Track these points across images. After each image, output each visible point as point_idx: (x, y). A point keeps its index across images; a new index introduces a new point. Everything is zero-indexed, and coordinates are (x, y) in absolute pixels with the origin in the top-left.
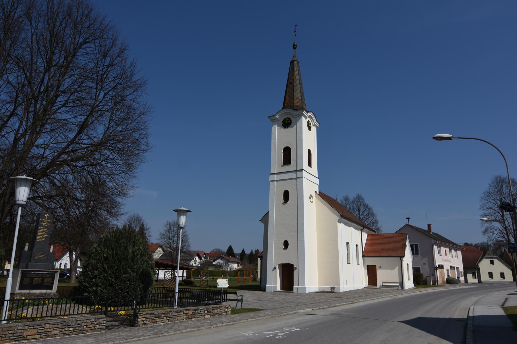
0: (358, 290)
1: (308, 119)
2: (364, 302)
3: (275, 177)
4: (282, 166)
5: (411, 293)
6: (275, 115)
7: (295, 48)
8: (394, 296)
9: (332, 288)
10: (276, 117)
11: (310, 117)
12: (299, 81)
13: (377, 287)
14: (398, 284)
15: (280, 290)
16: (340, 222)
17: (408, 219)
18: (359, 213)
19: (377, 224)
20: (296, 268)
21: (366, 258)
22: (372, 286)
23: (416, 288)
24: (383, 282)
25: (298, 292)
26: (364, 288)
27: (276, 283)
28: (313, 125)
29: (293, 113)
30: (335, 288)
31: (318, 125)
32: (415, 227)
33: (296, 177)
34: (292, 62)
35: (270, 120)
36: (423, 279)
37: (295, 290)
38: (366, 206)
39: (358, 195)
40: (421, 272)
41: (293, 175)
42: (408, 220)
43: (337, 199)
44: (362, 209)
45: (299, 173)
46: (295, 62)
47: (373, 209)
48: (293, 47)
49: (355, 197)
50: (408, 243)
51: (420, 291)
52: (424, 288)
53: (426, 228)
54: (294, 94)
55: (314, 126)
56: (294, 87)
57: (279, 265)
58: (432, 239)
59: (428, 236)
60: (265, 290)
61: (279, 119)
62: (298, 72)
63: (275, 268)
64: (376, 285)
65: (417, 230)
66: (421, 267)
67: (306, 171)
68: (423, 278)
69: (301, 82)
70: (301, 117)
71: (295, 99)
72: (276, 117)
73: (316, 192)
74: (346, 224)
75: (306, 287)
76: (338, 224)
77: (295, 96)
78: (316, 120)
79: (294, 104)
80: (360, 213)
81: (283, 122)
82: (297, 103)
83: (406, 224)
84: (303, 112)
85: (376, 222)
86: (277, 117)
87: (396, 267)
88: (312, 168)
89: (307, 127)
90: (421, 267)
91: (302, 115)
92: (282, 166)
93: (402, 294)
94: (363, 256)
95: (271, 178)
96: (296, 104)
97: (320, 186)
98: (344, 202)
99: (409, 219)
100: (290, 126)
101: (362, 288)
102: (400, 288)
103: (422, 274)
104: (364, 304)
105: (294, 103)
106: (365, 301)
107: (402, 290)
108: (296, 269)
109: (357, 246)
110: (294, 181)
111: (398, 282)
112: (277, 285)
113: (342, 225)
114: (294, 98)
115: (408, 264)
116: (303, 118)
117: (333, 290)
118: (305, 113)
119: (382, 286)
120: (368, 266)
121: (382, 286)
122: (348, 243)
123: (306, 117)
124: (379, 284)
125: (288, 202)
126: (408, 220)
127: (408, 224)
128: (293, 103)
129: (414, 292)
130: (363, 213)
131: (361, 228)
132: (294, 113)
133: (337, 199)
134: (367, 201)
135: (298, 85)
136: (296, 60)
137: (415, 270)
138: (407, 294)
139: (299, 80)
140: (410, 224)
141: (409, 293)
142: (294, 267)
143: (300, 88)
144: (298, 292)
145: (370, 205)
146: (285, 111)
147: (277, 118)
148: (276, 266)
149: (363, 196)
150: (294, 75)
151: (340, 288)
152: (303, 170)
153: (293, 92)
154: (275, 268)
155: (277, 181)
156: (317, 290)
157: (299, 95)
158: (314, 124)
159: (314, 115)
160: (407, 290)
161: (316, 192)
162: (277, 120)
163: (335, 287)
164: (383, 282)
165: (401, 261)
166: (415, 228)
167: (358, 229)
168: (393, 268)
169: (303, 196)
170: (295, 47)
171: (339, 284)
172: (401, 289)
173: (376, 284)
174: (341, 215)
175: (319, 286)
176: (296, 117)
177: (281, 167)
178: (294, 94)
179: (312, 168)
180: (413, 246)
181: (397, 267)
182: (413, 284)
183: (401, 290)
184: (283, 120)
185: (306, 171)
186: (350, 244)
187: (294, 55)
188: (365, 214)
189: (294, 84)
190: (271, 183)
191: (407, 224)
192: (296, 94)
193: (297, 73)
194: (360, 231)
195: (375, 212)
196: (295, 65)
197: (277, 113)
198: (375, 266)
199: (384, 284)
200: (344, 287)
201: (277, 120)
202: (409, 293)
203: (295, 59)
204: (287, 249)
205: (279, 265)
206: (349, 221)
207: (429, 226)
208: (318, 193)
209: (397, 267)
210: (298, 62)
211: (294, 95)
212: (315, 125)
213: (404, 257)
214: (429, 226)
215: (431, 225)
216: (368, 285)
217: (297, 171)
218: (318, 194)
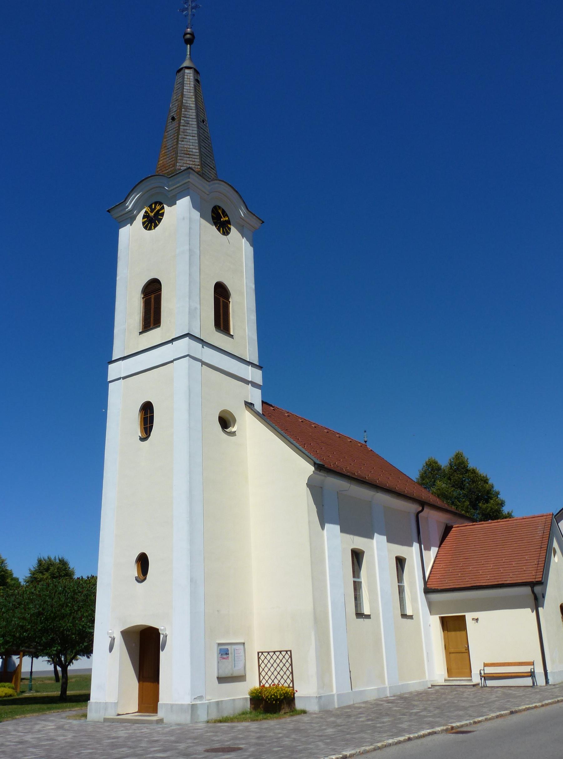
24: (486, 665)
94: (427, 591)
100: (159, 222)
144: (547, 682)
179: (232, 336)
205: (126, 634)
208: (258, 407)
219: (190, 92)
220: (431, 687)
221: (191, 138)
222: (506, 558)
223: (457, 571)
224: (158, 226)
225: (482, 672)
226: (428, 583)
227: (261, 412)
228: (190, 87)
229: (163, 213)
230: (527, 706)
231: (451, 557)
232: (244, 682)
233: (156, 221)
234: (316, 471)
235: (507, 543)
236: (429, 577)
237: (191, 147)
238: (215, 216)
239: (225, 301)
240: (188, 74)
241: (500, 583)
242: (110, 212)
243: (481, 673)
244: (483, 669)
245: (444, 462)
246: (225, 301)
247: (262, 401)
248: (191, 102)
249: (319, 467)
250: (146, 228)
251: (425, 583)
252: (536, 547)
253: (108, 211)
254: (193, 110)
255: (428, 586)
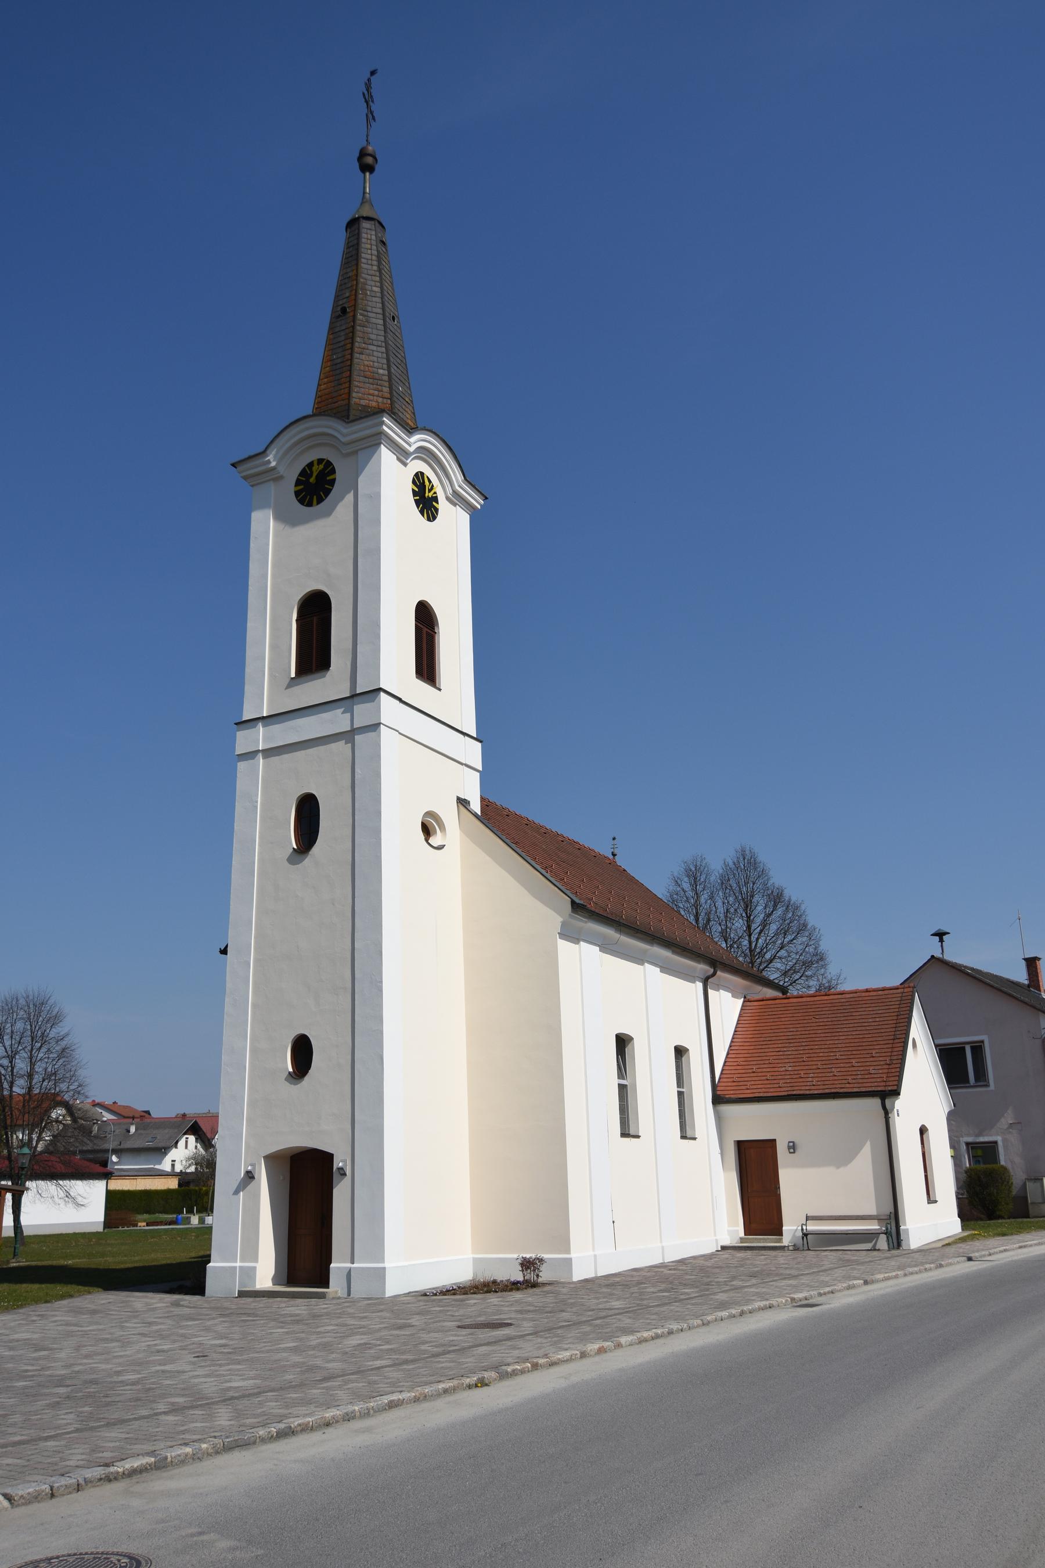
0: (682, 1262)
1: (417, 466)
2: (586, 1362)
3: (261, 737)
4: (292, 682)
5: (920, 1272)
6: (264, 453)
7: (366, 168)
8: (820, 1295)
9: (527, 1264)
10: (269, 462)
11: (424, 453)
12: (383, 303)
13: (780, 1241)
14: (874, 1226)
15: (276, 1280)
16: (570, 935)
17: (940, 935)
18: (749, 927)
19: (824, 966)
20: (342, 1173)
21: (727, 1109)
22: (759, 1241)
23: (972, 1238)
24: (808, 1218)
25: (349, 1294)
26: (724, 1248)
27: (252, 1252)
28: (448, 498)
29: (336, 434)
30: (541, 1260)
31: (477, 502)
32: (972, 969)
33: (349, 729)
34: (353, 224)
35: (245, 478)
36: (1010, 1191)
37: (336, 1285)
38: (776, 898)
39: (743, 851)
40: (1003, 1163)
41: (337, 721)
42: (941, 941)
43: (614, 855)
44: (760, 908)
45: (362, 713)
46: (365, 225)
47: (803, 907)
48: (357, 165)
49: (731, 864)
50: (918, 1029)
51: (970, 1259)
52: (1004, 1235)
53: (1021, 976)
54: (356, 355)
55: (455, 505)
56: (353, 327)
57: (272, 1160)
58: (1040, 1013)
59: (1026, 1003)
60: (199, 1289)
61: (281, 470)
62: (379, 267)
63: (250, 1176)
64: (778, 1231)
65: (975, 978)
66: (1004, 1140)
67: (400, 700)
68: (1009, 1185)
69: (389, 306)
70: (378, 449)
71: (357, 380)
72: (269, 462)
73: (463, 802)
74: (606, 947)
75: (387, 1265)
76: (563, 946)
77: (356, 367)
78: (460, 477)
79: (354, 401)
80: (754, 926)
81: (298, 483)
82: (363, 394)
83: (930, 957)
84: (383, 423)
85: (820, 958)
86: (271, 459)
87: (865, 1144)
88: (440, 690)
89: (410, 500)
90: (999, 1139)
91: (376, 439)
92: (292, 682)
93: (866, 1283)
94: (718, 1100)
95: (244, 740)
96: (363, 402)
97: (486, 777)
98: (686, 886)
99: (945, 938)
100: (327, 495)
101: (710, 1248)
102: (882, 1242)
103: (1005, 1169)
104: (562, 1383)
105: (354, 395)
106: (601, 1351)
107: (895, 1252)
108: (345, 1174)
109: (680, 1052)
110: (341, 748)
111: (873, 1211)
112: (256, 1259)
113: (589, 951)
114: (355, 377)
115: (923, 1131)
116: (386, 456)
117: (531, 1276)
118: (389, 427)
119: (805, 1235)
120: (740, 1145)
121: (805, 1235)
122: (623, 1042)
123: (403, 455)
124: (791, 1229)
125: (316, 849)
126: (941, 941)
127: (938, 954)
128: (349, 393)
129: (941, 1266)
130: (764, 924)
131: (703, 968)
132: (344, 435)
133: (614, 855)
134: (778, 878)
135: (374, 320)
136: (375, 217)
137: (979, 1153)
138: (896, 1277)
139: (379, 300)
140: (948, 957)
141: (911, 1270)
142: (338, 1163)
143: (385, 332)
144: (349, 1294)
145: (792, 893)
146: (307, 429)
147: (273, 464)
148: (253, 1165)
149: (763, 857)
150: (357, 276)
151: (569, 1261)
152: (380, 689)
153: (352, 349)
154: (250, 1176)
155: (268, 753)
156: (462, 1274)
157: (376, 364)
158: (455, 493)
159: (450, 448)
160: (919, 1250)
161: (463, 802)
162: (272, 476)
163: (545, 1256)
164: (808, 1218)
165: (887, 1112)
166: (968, 974)
167: (687, 976)
168: (843, 1158)
169: (379, 813)
170: (369, 160)
171: (564, 1244)
172: (889, 1250)
173: (776, 1229)
174: (573, 903)
175: (473, 1253)
176: (356, 452)
177: (286, 689)
178: (351, 360)
179: (440, 690)
180: (964, 1048)
181: (868, 1144)
182: (957, 1222)
183: (888, 1254)
184: (300, 475)
185: (400, 700)
186: (639, 1050)
187: (364, 197)
188: (774, 927)
189: (354, 316)
190: (242, 766)
191: (933, 956)
192: (363, 357)
193: (375, 268)
194: (700, 985)
195: (812, 921)
196: (364, 235)
197: (272, 442)
198: (772, 1143)
199: (812, 1227)
200: (595, 1256)
201: (272, 476)
202: (911, 1270)
203: (366, 212)
204: (306, 1078)
205: (272, 1160)
206: (620, 932)
207: (1031, 963)
208: (476, 806)
209: (868, 1144)
210: (383, 227)
211: (355, 361)
212: (457, 499)
213: (896, 1093)
214: (1031, 963)
215: (1039, 959)
216: (742, 1234)
217: (356, 699)
218: (475, 815)
219: (373, 264)
220: (720, 1249)
221: (375, 348)
222: (842, 1053)
223: (764, 1070)
224: (325, 501)
225: (804, 1227)
226: (719, 1088)
227: (480, 814)
228: (372, 255)
229: (334, 480)
230: (886, 1275)
231: (752, 1047)
232: (909, 1230)
233: (304, 479)
234: (572, 914)
235: (824, 1009)
236: (720, 1078)
237: (376, 364)
238: (417, 490)
239: (430, 632)
240: (369, 231)
241: (833, 1091)
242: (236, 468)
243: (802, 1229)
244: (805, 1223)
245: (716, 863)
246: (430, 632)
247: (482, 798)
248: (373, 283)
249: (576, 907)
250: (301, 502)
251: (714, 1086)
252: (887, 1038)
253: (233, 465)
254: (377, 298)
255: (719, 1093)
